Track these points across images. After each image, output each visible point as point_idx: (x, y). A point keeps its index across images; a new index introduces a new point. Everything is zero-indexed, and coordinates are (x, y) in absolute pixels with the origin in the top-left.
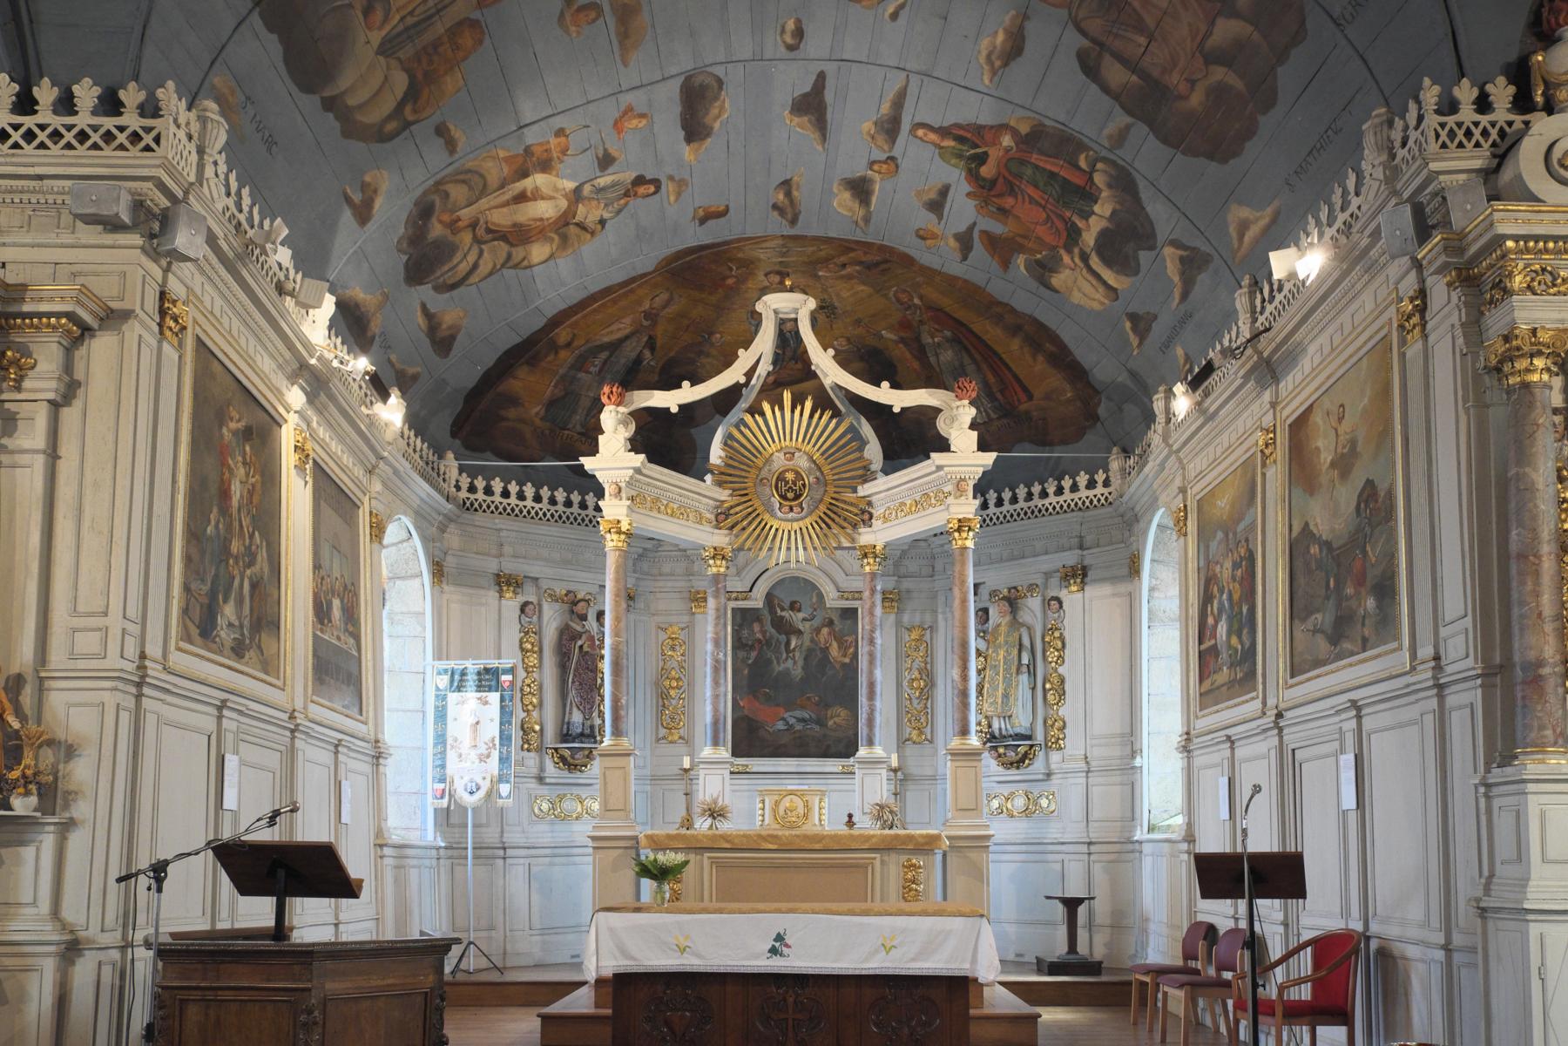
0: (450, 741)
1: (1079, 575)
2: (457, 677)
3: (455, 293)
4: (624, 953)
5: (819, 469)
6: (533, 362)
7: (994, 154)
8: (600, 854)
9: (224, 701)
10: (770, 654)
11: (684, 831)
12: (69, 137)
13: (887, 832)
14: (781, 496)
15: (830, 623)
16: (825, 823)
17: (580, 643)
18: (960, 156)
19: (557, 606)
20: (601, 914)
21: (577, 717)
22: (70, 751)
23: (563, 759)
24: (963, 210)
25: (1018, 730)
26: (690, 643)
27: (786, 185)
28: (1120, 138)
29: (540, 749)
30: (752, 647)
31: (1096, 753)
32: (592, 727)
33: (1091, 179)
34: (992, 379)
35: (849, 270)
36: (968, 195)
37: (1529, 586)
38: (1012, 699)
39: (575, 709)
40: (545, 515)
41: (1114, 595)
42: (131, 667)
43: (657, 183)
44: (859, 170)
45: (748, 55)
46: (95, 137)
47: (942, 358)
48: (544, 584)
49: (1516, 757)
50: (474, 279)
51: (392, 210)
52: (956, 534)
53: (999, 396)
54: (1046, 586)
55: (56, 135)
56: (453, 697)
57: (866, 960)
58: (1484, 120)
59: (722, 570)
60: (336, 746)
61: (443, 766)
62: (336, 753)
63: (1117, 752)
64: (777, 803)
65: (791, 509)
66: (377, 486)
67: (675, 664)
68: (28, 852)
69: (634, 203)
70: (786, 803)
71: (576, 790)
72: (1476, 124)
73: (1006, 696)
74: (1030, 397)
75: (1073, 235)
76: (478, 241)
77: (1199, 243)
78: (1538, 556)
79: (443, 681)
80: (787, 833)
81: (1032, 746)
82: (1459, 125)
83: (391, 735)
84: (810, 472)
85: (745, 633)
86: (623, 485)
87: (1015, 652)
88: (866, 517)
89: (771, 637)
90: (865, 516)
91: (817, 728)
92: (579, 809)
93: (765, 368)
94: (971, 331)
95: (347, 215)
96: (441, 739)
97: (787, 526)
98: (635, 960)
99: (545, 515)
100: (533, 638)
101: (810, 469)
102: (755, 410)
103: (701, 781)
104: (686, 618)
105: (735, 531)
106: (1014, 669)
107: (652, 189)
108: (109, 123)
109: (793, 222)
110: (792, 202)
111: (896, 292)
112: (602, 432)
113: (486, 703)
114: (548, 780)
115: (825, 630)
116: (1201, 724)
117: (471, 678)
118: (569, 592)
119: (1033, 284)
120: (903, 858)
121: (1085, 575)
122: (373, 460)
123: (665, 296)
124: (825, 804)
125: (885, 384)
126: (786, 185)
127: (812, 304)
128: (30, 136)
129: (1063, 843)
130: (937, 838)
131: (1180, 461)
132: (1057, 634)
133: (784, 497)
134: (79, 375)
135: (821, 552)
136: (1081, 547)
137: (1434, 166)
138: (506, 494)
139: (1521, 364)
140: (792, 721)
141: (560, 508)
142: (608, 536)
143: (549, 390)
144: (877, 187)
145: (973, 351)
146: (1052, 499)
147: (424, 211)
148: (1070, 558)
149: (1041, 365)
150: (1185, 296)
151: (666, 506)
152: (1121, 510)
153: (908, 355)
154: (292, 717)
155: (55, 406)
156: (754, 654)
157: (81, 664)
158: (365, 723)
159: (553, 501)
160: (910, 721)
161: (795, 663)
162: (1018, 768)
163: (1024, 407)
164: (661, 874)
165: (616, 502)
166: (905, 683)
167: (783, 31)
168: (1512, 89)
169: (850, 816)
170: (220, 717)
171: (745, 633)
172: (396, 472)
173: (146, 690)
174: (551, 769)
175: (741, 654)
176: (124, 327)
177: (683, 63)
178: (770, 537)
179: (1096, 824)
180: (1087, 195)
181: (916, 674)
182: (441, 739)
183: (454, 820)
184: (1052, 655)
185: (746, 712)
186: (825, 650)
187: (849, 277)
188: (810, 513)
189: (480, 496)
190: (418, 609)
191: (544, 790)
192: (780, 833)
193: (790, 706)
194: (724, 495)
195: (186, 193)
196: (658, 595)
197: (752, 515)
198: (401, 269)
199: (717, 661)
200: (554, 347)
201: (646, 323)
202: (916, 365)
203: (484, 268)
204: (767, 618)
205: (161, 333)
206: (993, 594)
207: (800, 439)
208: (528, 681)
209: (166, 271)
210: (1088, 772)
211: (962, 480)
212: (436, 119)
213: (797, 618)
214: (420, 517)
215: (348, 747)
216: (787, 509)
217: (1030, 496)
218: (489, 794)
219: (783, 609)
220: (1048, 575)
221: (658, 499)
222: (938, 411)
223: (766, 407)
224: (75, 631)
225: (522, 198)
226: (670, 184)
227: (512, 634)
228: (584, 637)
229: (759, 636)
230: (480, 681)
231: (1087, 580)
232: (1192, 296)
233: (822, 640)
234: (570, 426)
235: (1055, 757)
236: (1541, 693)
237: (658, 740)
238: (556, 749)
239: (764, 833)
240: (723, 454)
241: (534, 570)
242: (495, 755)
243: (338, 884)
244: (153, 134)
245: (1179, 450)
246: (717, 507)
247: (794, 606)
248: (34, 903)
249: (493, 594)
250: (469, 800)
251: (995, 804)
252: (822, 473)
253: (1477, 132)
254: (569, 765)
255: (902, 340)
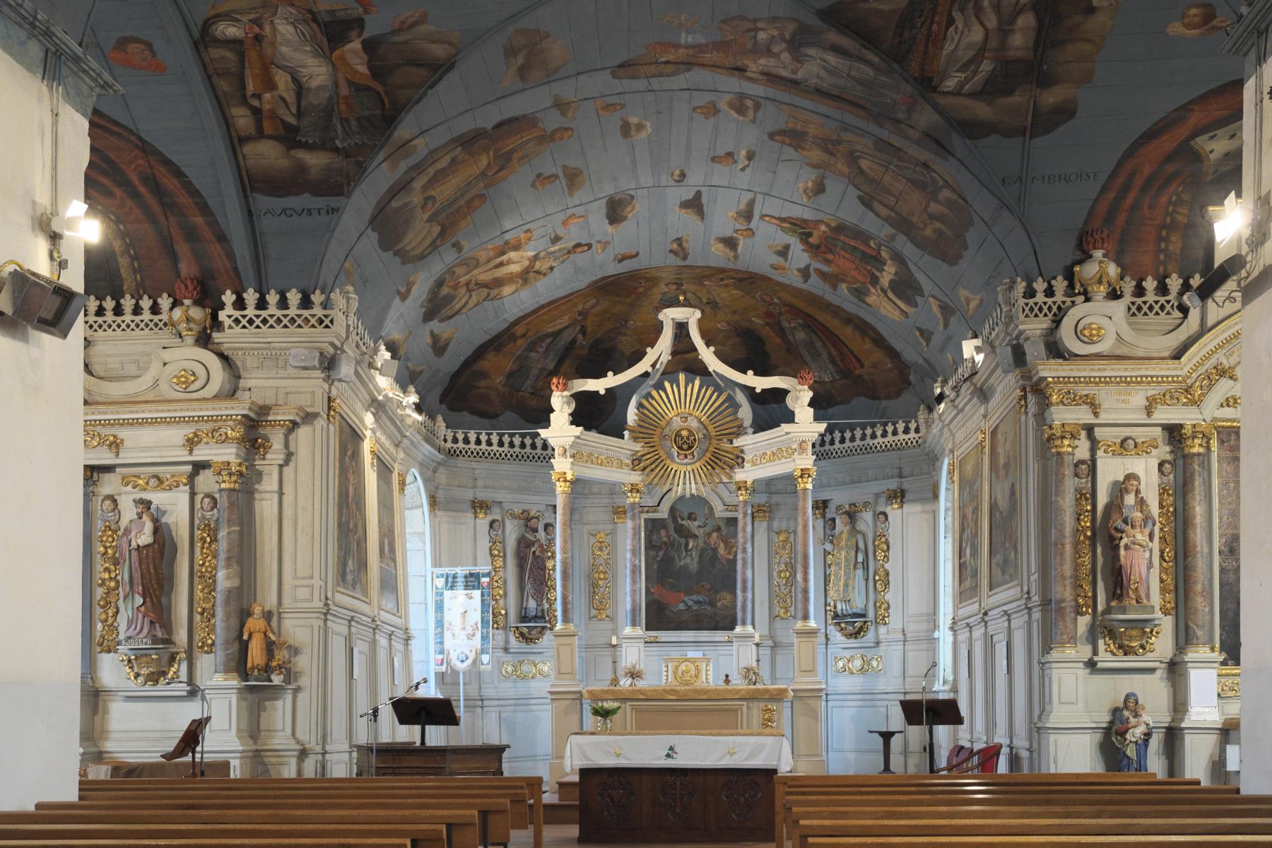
0: (446, 625)
1: (899, 496)
2: (450, 580)
3: (452, 321)
4: (586, 757)
5: (706, 428)
6: (498, 349)
7: (816, 233)
8: (556, 703)
9: (353, 617)
10: (673, 553)
11: (613, 688)
12: (285, 321)
13: (752, 687)
14: (678, 447)
15: (719, 529)
16: (711, 680)
17: (533, 549)
18: (794, 232)
19: (516, 522)
20: (573, 736)
21: (532, 604)
22: (295, 651)
23: (522, 634)
24: (800, 256)
25: (855, 611)
26: (613, 545)
27: (679, 241)
28: (892, 238)
29: (505, 628)
30: (660, 548)
31: (911, 628)
32: (543, 611)
33: (879, 253)
34: (834, 352)
35: (726, 282)
36: (803, 250)
37: (1058, 560)
38: (850, 588)
39: (530, 599)
40: (506, 455)
41: (923, 512)
42: (321, 604)
43: (590, 246)
44: (728, 232)
45: (650, 184)
46: (299, 321)
47: (797, 337)
48: (506, 506)
49: (1051, 649)
50: (464, 310)
51: (421, 288)
52: (800, 480)
53: (840, 363)
54: (876, 503)
55: (279, 321)
56: (448, 594)
57: (720, 759)
58: (1050, 301)
59: (637, 500)
60: (390, 635)
61: (442, 643)
62: (390, 640)
63: (924, 626)
64: (677, 668)
65: (686, 457)
66: (401, 455)
67: (603, 562)
68: (279, 703)
69: (572, 256)
70: (683, 667)
71: (531, 657)
72: (1045, 303)
73: (846, 585)
74: (862, 366)
75: (875, 281)
76: (469, 290)
77: (947, 300)
78: (1063, 545)
79: (440, 583)
80: (683, 688)
81: (865, 622)
82: (1036, 304)
83: (415, 625)
84: (698, 430)
85: (655, 537)
86: (567, 447)
87: (853, 553)
88: (740, 461)
89: (674, 540)
90: (739, 459)
91: (709, 608)
92: (534, 671)
93: (666, 358)
94: (816, 320)
95: (397, 299)
96: (440, 624)
97: (683, 468)
98: (590, 760)
99: (506, 455)
100: (499, 546)
101: (699, 428)
102: (659, 386)
103: (624, 649)
104: (610, 527)
105: (646, 472)
106: (852, 566)
107: (586, 248)
108: (306, 313)
109: (685, 258)
110: (683, 249)
111: (760, 296)
112: (552, 411)
113: (471, 598)
114: (512, 650)
115: (715, 535)
116: (963, 612)
117: (460, 580)
118: (524, 511)
119: (855, 300)
120: (762, 705)
121: (903, 496)
122: (399, 438)
123: (593, 302)
124: (711, 667)
125: (750, 372)
126: (679, 241)
127: (698, 314)
128: (265, 321)
129: (887, 693)
130: (786, 690)
131: (951, 431)
132: (883, 540)
133: (680, 448)
134: (292, 449)
135: (709, 487)
136: (900, 476)
137: (1021, 327)
138: (478, 442)
139: (1058, 442)
140: (690, 603)
141: (517, 449)
142: (558, 483)
143: (509, 365)
144: (741, 242)
145: (820, 333)
146: (880, 440)
147: (440, 283)
148: (893, 484)
149: (868, 345)
150: (946, 326)
151: (597, 458)
152: (927, 450)
153: (773, 334)
154: (373, 621)
155: (281, 466)
156: (661, 553)
157: (300, 605)
158: (401, 617)
159: (512, 445)
160: (778, 602)
161: (692, 559)
162: (856, 638)
163: (857, 372)
164: (605, 714)
165: (562, 459)
166: (775, 574)
167: (672, 175)
168: (1066, 283)
169: (727, 676)
170: (350, 626)
171: (655, 537)
172: (412, 443)
173: (329, 617)
174: (513, 642)
175: (652, 553)
176: (315, 422)
177: (609, 190)
178: (671, 476)
179: (911, 679)
180: (879, 262)
181: (783, 567)
182: (440, 624)
183: (447, 680)
184: (880, 555)
185: (656, 597)
186: (715, 550)
187: (726, 286)
188: (699, 459)
189: (461, 445)
190: (421, 531)
191: (509, 657)
192: (679, 688)
193: (689, 592)
194: (638, 447)
195: (342, 344)
196: (589, 509)
197: (658, 461)
198: (421, 315)
199: (634, 566)
200: (513, 338)
201: (579, 318)
202: (778, 340)
203: (471, 304)
204: (671, 526)
205: (328, 419)
206: (839, 508)
207: (692, 407)
208: (496, 578)
209: (330, 385)
210: (905, 641)
211: (803, 442)
212: (454, 240)
213: (693, 525)
214: (422, 466)
215: (335, 615)
216: (682, 457)
217: (863, 438)
218: (474, 662)
219: (683, 519)
220: (877, 495)
221: (591, 454)
222: (785, 392)
223: (667, 385)
224: (296, 587)
225: (501, 265)
226: (599, 245)
227: (484, 544)
228: (536, 545)
229: (665, 539)
230: (467, 582)
231: (905, 500)
232: (950, 327)
233: (712, 542)
234: (523, 389)
235: (882, 630)
236: (1063, 616)
237: (590, 619)
238: (517, 628)
239: (668, 688)
240: (636, 418)
241: (499, 496)
242: (478, 634)
243: (451, 719)
244: (330, 318)
245: (949, 425)
246: (633, 455)
247: (691, 517)
248: (283, 730)
249: (470, 515)
250: (461, 667)
251: (841, 664)
252: (707, 430)
253: (1045, 308)
254: (527, 639)
255: (767, 324)
